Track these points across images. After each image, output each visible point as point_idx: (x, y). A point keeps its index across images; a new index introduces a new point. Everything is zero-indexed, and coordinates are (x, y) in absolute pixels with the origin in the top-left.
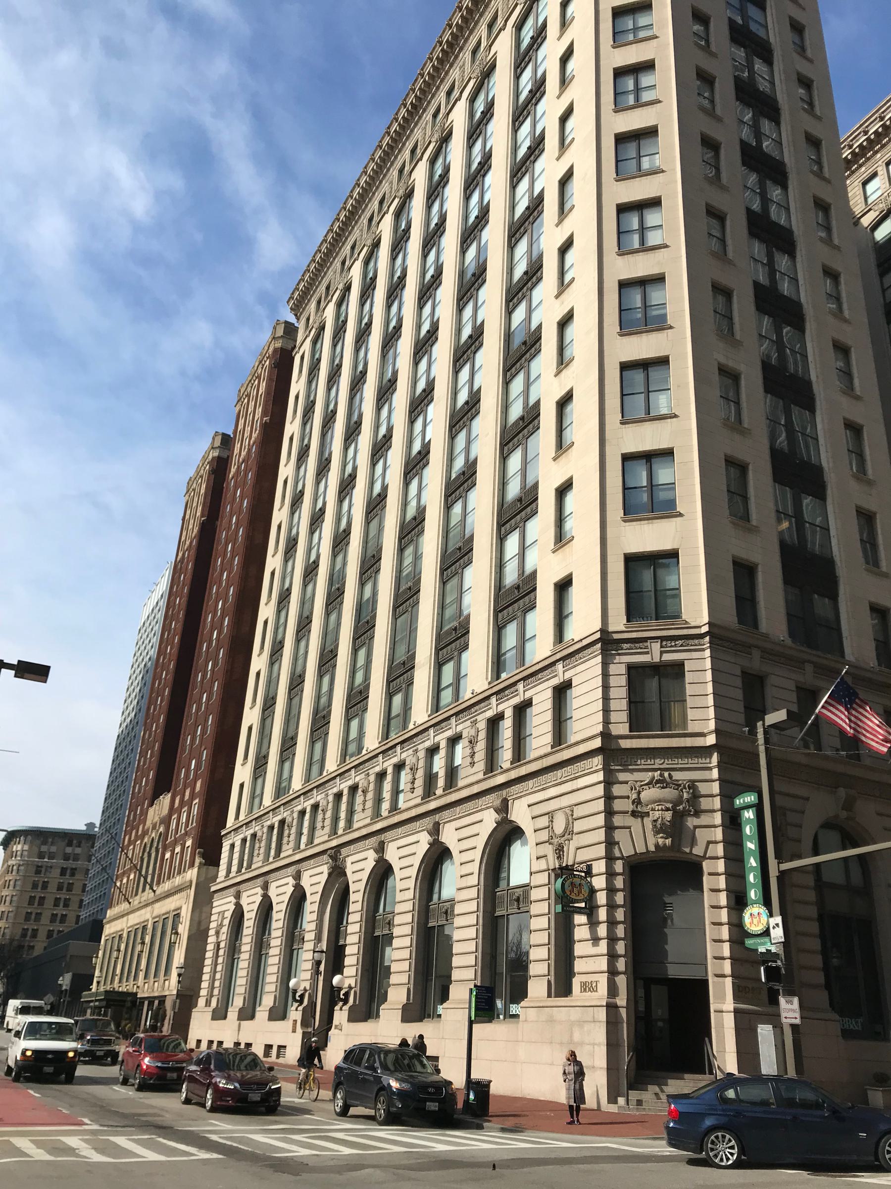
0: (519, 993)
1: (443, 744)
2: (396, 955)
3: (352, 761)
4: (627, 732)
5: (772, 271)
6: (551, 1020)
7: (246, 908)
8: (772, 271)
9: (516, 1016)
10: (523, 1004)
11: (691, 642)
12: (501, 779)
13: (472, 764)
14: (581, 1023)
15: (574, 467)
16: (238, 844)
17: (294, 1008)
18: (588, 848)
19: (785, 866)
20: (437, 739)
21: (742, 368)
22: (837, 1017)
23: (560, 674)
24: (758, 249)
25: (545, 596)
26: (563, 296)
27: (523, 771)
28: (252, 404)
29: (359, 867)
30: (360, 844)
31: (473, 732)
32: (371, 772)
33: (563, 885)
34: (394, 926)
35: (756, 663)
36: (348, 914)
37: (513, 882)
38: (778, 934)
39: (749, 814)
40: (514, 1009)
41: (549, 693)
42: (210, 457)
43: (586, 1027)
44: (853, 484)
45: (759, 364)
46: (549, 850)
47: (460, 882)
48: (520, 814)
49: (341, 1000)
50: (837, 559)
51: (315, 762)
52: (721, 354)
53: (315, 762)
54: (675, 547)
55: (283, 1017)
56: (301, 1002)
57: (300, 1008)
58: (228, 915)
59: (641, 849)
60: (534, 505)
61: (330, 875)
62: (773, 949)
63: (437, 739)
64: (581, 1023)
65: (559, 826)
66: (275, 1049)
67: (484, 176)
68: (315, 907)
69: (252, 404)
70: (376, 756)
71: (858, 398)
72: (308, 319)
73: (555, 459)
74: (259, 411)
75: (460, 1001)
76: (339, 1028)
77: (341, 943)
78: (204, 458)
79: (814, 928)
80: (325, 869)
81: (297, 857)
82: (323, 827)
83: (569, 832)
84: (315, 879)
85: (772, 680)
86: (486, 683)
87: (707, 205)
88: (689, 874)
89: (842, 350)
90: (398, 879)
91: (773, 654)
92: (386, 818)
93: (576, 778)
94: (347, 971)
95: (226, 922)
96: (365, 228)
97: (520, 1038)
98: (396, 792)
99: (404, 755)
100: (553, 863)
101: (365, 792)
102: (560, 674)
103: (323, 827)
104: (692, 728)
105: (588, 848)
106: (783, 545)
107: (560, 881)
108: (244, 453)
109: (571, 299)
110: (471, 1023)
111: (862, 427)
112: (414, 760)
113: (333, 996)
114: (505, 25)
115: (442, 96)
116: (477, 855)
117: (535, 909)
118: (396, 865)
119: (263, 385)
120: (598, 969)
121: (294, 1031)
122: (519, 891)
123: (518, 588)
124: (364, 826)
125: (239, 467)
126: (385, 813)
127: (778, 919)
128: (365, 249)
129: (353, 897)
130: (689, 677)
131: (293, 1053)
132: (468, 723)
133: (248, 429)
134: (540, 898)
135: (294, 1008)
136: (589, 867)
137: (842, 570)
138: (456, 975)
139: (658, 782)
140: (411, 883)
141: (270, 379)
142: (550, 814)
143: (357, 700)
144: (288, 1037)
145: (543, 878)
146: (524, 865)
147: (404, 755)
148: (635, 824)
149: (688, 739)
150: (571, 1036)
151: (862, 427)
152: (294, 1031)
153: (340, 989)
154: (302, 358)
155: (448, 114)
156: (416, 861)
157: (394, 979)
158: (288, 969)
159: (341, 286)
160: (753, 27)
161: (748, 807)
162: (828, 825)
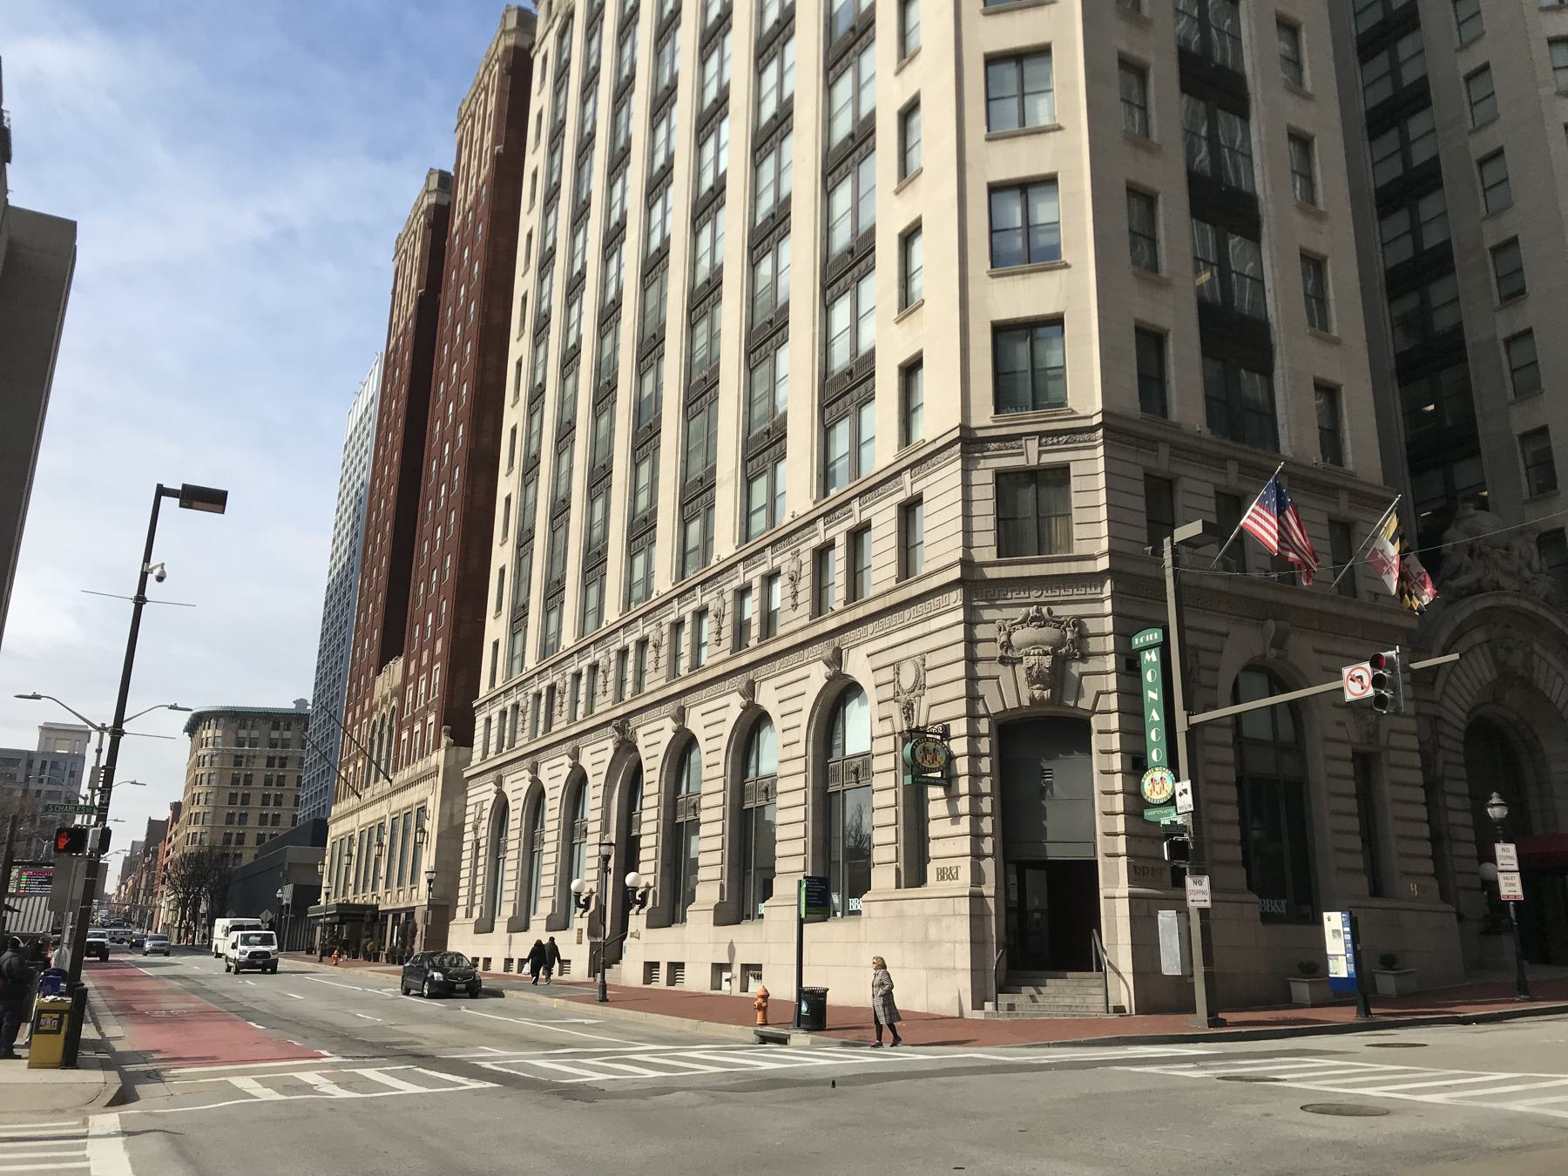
0: (860, 885)
3: (638, 609)
6: (901, 916)
9: (858, 913)
10: (865, 897)
11: (1079, 437)
12: (832, 624)
13: (795, 606)
14: (938, 918)
15: (922, 200)
22: (1255, 897)
23: (907, 487)
25: (887, 382)
27: (860, 612)
28: (478, 128)
29: (654, 739)
30: (655, 712)
33: (913, 751)
38: (1185, 802)
40: (854, 904)
41: (892, 513)
42: (425, 204)
44: (1298, 218)
46: (895, 709)
48: (857, 666)
49: (637, 902)
51: (590, 612)
52: (1123, 40)
54: (1059, 310)
56: (586, 907)
58: (488, 805)
59: (1011, 703)
61: (617, 750)
62: (1180, 820)
63: (748, 576)
64: (938, 918)
65: (907, 679)
68: (600, 791)
69: (478, 128)
70: (670, 601)
71: (1308, 97)
75: (786, 898)
77: (635, 833)
80: (610, 745)
82: (605, 692)
83: (920, 686)
84: (597, 757)
85: (1184, 484)
91: (1186, 450)
94: (643, 868)
95: (486, 814)
98: (698, 645)
99: (706, 599)
100: (900, 724)
101: (657, 646)
102: (907, 487)
104: (1079, 549)
105: (944, 704)
107: (909, 746)
108: (470, 198)
112: (719, 604)
113: (627, 899)
116: (803, 718)
117: (877, 782)
119: (492, 101)
121: (579, 942)
123: (850, 373)
125: (465, 218)
126: (683, 672)
127: (1187, 784)
129: (647, 777)
130: (1075, 484)
133: (475, 163)
136: (946, 729)
137: (1279, 337)
138: (780, 866)
142: (896, 666)
143: (641, 530)
145: (888, 744)
146: (862, 729)
148: (1005, 673)
149: (1073, 564)
150: (926, 933)
152: (579, 942)
154: (545, 59)
156: (727, 729)
161: (1149, 647)
162: (1250, 668)
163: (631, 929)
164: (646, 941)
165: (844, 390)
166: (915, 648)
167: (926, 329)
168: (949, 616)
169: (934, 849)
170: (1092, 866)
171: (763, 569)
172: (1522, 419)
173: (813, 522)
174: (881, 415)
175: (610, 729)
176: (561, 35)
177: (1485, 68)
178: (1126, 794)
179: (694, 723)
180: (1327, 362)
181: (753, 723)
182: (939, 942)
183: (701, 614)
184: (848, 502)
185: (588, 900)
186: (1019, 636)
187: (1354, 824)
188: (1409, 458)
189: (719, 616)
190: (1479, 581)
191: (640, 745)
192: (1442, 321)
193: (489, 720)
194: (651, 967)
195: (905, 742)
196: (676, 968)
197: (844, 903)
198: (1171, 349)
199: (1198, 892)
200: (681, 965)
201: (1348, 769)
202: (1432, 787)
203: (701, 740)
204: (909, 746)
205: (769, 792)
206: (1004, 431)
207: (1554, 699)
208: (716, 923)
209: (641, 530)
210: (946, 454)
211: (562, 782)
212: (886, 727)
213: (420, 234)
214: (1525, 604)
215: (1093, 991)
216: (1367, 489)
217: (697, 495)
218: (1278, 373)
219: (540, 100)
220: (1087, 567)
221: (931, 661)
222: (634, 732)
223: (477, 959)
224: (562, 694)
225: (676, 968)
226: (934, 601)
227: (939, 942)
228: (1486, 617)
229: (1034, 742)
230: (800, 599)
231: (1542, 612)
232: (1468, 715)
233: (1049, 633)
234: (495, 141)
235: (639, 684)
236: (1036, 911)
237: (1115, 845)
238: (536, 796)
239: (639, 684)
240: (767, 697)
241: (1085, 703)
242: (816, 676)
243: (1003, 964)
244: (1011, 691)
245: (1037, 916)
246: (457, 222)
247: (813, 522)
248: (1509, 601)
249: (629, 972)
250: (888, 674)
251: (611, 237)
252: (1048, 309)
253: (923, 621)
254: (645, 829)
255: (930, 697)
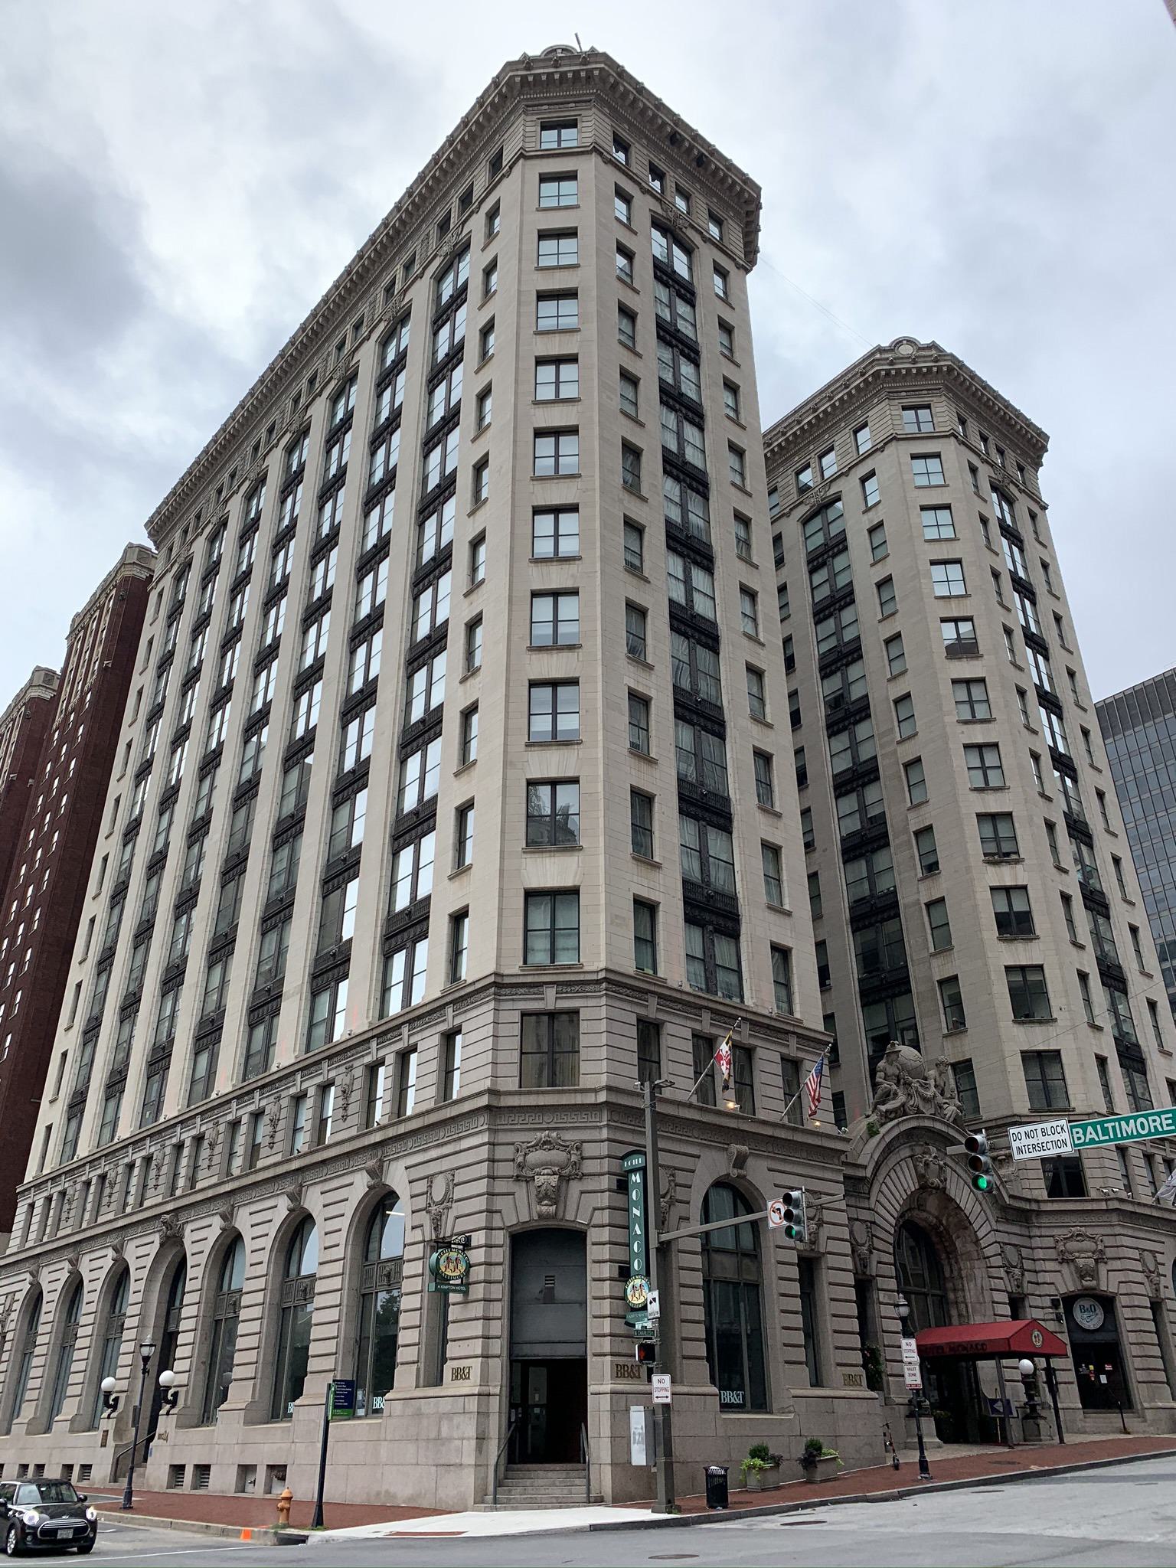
0: (384, 1382)
1: (311, 1092)
2: (252, 1356)
3: (200, 1105)
4: (516, 1088)
5: (689, 589)
6: (418, 1414)
7: (46, 1288)
8: (689, 589)
9: (378, 1411)
10: (388, 1396)
11: (588, 988)
12: (377, 1137)
13: (344, 1118)
14: (450, 1415)
15: (476, 780)
16: (39, 1203)
17: (105, 1415)
18: (467, 1215)
19: (664, 1237)
20: (305, 1085)
21: (652, 693)
22: (715, 1390)
23: (450, 1019)
24: (676, 565)
25: (439, 924)
26: (473, 596)
27: (402, 1129)
28: (89, 640)
29: (201, 1238)
30: (204, 1208)
31: (347, 1080)
32: (221, 1120)
33: (438, 1260)
34: (241, 1308)
35: (652, 1011)
36: (183, 1294)
37: (385, 1254)
38: (654, 1308)
39: (636, 1178)
40: (378, 1402)
41: (436, 1040)
42: (27, 697)
43: (457, 1419)
44: (759, 816)
45: (671, 688)
46: (425, 1219)
47: (325, 1255)
48: (397, 1177)
49: (168, 1402)
50: (740, 896)
51: (153, 1104)
52: (632, 678)
53: (153, 1104)
54: (577, 883)
55: (92, 1427)
56: (115, 1407)
57: (114, 1415)
58: (20, 1296)
59: (524, 1217)
60: (438, 728)
61: (162, 1245)
62: (649, 1325)
63: (305, 1085)
64: (450, 1415)
65: (438, 1194)
66: (189, 1472)
67: (392, 434)
68: (141, 1285)
69: (89, 640)
70: (229, 1101)
71: (770, 726)
72: (171, 550)
73: (456, 775)
74: (99, 650)
75: (317, 1396)
76: (164, 1437)
77: (172, 1329)
78: (18, 698)
79: (699, 1296)
80: (156, 1238)
81: (120, 1223)
82: (156, 1187)
83: (448, 1199)
84: (142, 1252)
85: (669, 1028)
86: (366, 1022)
87: (625, 516)
88: (574, 1239)
89: (755, 672)
90: (248, 1250)
91: (672, 1000)
92: (238, 1177)
93: (460, 1138)
94: (178, 1365)
95: (17, 1306)
96: (249, 458)
97: (382, 1436)
98: (254, 1149)
99: (263, 1103)
100: (429, 1234)
101: (212, 1146)
102: (450, 1019)
103: (156, 1187)
104: (585, 1082)
105: (467, 1215)
106: (686, 883)
107: (435, 1255)
108: (74, 700)
109: (481, 602)
110: (327, 1423)
111: (772, 755)
112: (275, 1109)
113: (161, 1397)
114: (423, 273)
115: (348, 328)
116: (344, 1223)
117: (406, 1286)
118: (247, 1234)
119: (106, 619)
120: (472, 1354)
121: (104, 1445)
122: (391, 1266)
123: (409, 914)
124: (210, 1187)
125: (67, 717)
126: (236, 1172)
127: (656, 1294)
128: (247, 483)
129: (190, 1273)
130: (584, 1026)
131: (102, 1471)
132: (343, 1069)
133: (82, 671)
134: (413, 1273)
135: (105, 1415)
136: (469, 1239)
137: (745, 910)
138: (313, 1365)
139: (545, 1143)
140: (264, 1256)
141: (115, 613)
142: (430, 1178)
143: (209, 1034)
144: (96, 1453)
145: (418, 1251)
146: (400, 1234)
147: (263, 1103)
148: (521, 1190)
149: (579, 1096)
150: (439, 1431)
151: (772, 755)
152: (104, 1445)
153: (169, 1388)
154: (160, 595)
155: (354, 352)
156: (272, 1230)
157: (237, 1372)
158: (104, 1364)
159: (214, 520)
160: (682, 325)
161: (635, 1171)
162: (719, 1184)
163: (160, 1430)
164: (175, 1443)
165: (404, 929)
166: (446, 1164)
167: (474, 884)
168: (475, 1143)
169: (452, 1350)
170: (581, 1364)
171: (319, 1080)
172: (941, 969)
173: (368, 1041)
174: (429, 953)
175: (157, 1224)
176: (179, 578)
177: (908, 696)
178: (614, 1303)
179: (243, 1221)
180: (783, 924)
181: (298, 1227)
182: (450, 1439)
183: (257, 1115)
184: (399, 1026)
185: (116, 1400)
186: (535, 1157)
187: (798, 1321)
188: (861, 992)
189: (274, 1122)
190: (903, 1105)
191: (187, 1242)
192: (883, 885)
193: (32, 1206)
194: (178, 1470)
195: (433, 1249)
196: (203, 1470)
197: (370, 1403)
198: (661, 916)
199: (662, 1389)
200: (207, 1468)
201: (794, 1272)
202: (864, 1286)
203: (247, 1239)
204: (435, 1255)
205: (308, 1294)
206: (529, 979)
207: (962, 1206)
208: (246, 1423)
209: (209, 1034)
210: (482, 995)
211: (102, 1274)
212: (417, 1235)
213: (19, 721)
214: (939, 1126)
215: (577, 1482)
216: (812, 1034)
217: (264, 1006)
218: (743, 938)
219: (152, 628)
220: (590, 1099)
221: (460, 1176)
222: (182, 1229)
223: (69, 1468)
224: (112, 1185)
225: (203, 1470)
226: (465, 1123)
227: (450, 1439)
228: (910, 1135)
229: (544, 1249)
230: (351, 1109)
231: (952, 1132)
232: (897, 1220)
233: (558, 1156)
234: (105, 655)
235: (192, 1181)
236: (537, 1406)
237: (601, 1346)
238: (75, 1289)
239: (192, 1181)
240: (313, 1201)
241: (582, 1220)
242: (359, 1184)
243: (503, 1460)
244: (521, 1209)
245: (537, 1411)
246: (58, 719)
247: (368, 1041)
248: (927, 1124)
249: (155, 1473)
250: (422, 1186)
251: (208, 759)
252: (568, 882)
253: (454, 1140)
254: (184, 1325)
255: (458, 1209)
